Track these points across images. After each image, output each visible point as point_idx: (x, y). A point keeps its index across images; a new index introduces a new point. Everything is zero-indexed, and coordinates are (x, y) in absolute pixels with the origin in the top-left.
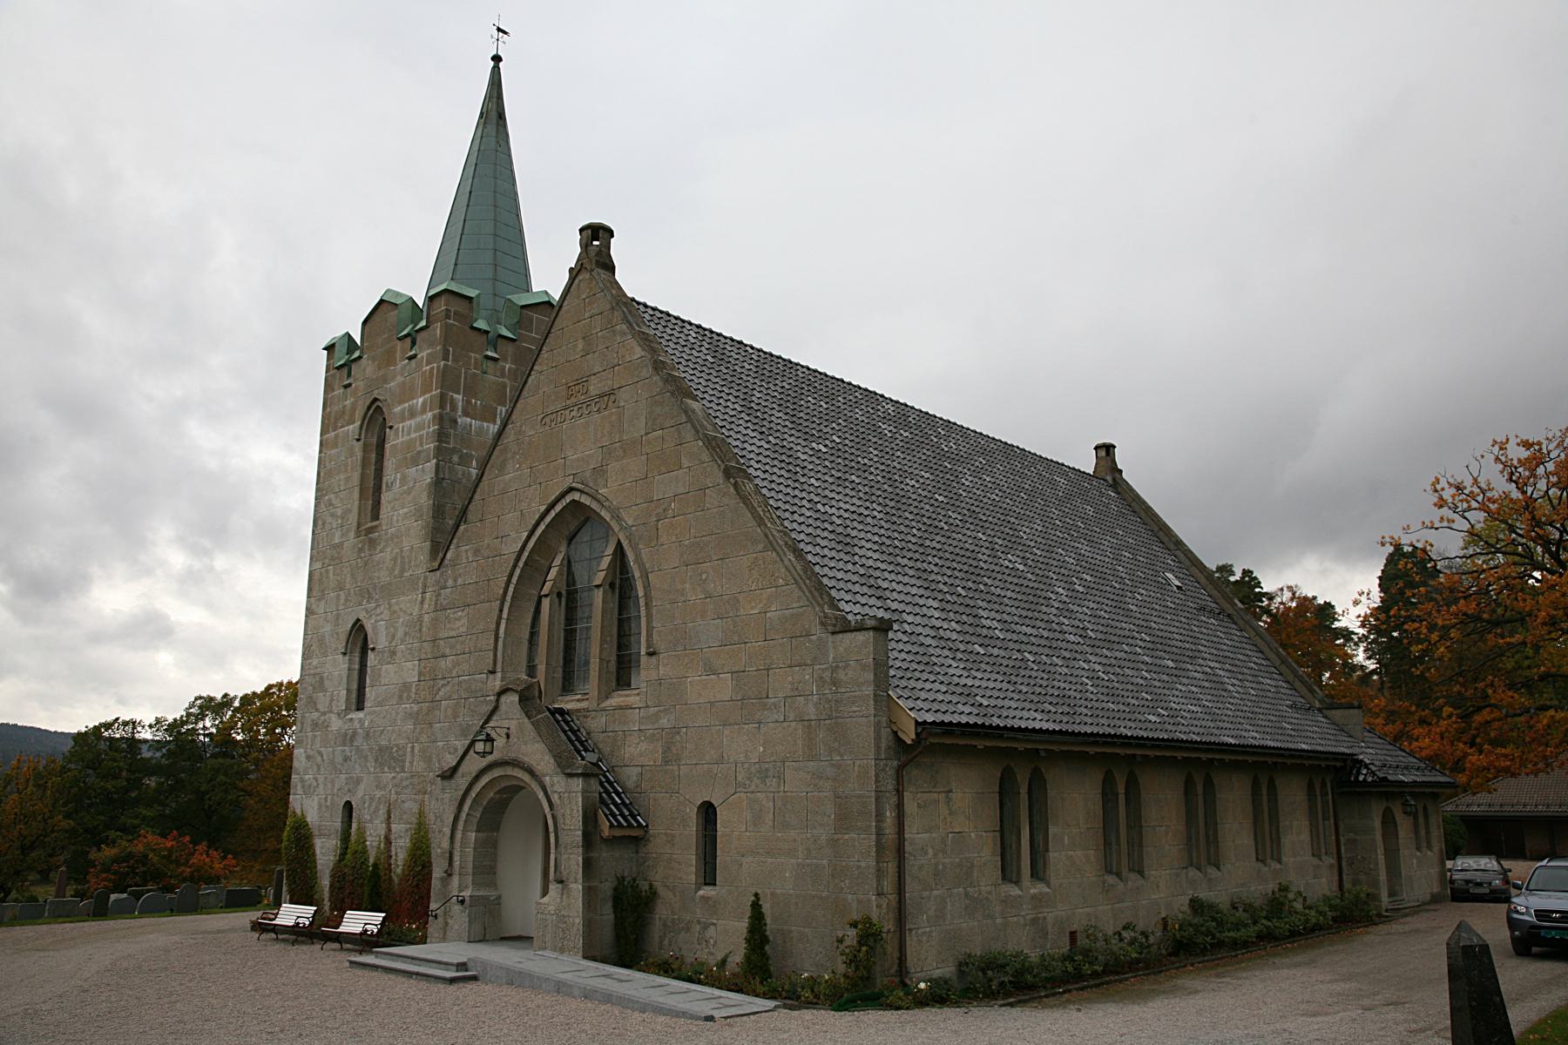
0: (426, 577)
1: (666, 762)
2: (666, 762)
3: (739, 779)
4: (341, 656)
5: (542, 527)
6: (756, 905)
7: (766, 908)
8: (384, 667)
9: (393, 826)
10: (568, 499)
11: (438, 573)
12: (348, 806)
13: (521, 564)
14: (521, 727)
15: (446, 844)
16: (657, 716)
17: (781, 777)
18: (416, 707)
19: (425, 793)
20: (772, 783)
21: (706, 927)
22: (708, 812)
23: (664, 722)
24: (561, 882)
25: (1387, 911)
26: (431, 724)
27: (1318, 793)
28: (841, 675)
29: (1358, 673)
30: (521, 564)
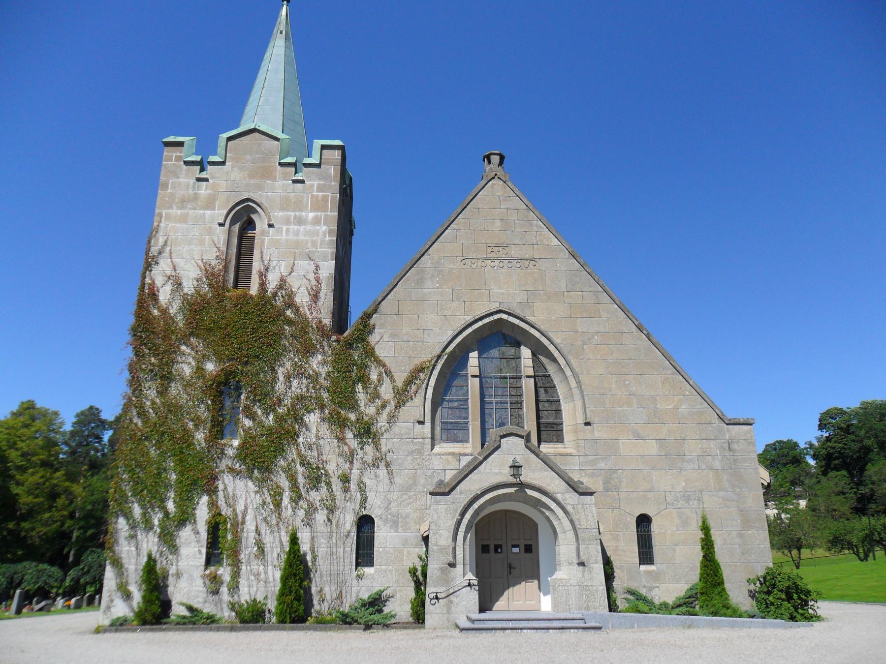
3: (669, 500)
10: (496, 317)
17: (700, 500)
23: (602, 465)
24: (581, 564)
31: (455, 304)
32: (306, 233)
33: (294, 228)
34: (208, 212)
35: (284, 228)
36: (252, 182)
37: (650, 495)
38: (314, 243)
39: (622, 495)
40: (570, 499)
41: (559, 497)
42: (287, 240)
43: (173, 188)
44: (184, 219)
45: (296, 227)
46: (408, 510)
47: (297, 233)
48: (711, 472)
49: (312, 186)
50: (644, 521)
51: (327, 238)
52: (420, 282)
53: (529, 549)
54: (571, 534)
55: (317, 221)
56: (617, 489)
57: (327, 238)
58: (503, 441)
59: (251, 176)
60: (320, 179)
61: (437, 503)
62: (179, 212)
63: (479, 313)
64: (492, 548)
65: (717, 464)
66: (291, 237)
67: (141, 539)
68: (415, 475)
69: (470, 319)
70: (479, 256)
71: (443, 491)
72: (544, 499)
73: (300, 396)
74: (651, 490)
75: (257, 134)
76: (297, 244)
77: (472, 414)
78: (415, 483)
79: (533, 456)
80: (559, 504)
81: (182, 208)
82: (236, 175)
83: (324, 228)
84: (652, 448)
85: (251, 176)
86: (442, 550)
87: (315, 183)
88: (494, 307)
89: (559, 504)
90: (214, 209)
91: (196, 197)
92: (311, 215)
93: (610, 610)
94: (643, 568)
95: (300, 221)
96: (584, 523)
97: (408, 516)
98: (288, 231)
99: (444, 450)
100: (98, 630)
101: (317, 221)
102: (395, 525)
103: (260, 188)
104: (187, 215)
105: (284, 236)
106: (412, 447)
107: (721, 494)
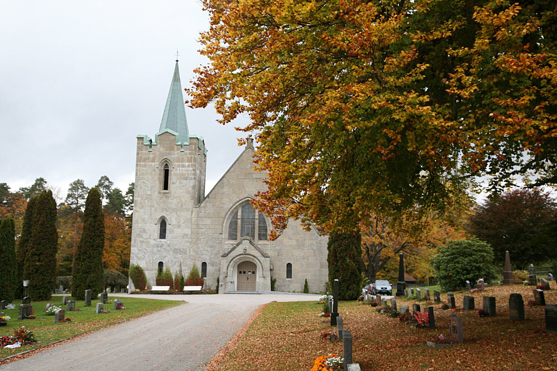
0: (192, 209)
1: (278, 255)
2: (278, 255)
3: (298, 259)
4: (154, 225)
5: (238, 204)
6: (306, 281)
7: (307, 281)
8: (175, 229)
9: (182, 268)
10: (247, 199)
11: (198, 209)
12: (161, 264)
13: (231, 211)
14: (250, 247)
15: (225, 270)
16: (275, 247)
17: (308, 259)
18: (190, 240)
19: (196, 260)
20: (306, 260)
21: (289, 285)
22: (289, 266)
23: (277, 248)
24: (264, 277)
25: (407, 291)
26: (197, 244)
27: (257, 222)
28: (322, 242)
29: (399, 137)
30: (231, 211)
31: (234, 194)
32: (186, 171)
33: (181, 168)
34: (153, 163)
35: (178, 168)
36: (167, 152)
37: (292, 257)
38: (188, 174)
39: (283, 257)
40: (262, 259)
41: (259, 258)
42: (179, 173)
43: (141, 154)
44: (145, 166)
45: (182, 168)
46: (217, 261)
47: (182, 171)
48: (312, 251)
49: (187, 153)
50: (289, 266)
51: (192, 172)
52: (222, 187)
53: (253, 273)
54: (261, 269)
55: (189, 166)
56: (281, 255)
57: (192, 172)
58: (243, 241)
59: (166, 150)
60: (190, 150)
61: (223, 259)
62: (143, 163)
63: (241, 198)
64: (242, 273)
65: (315, 248)
66: (181, 172)
67: (479, 287)
68: (219, 250)
69: (238, 200)
70: (242, 178)
71: (225, 256)
72: (254, 259)
73: (135, 270)
74: (293, 256)
75: (168, 134)
76: (183, 174)
77: (56, 296)
78: (219, 253)
79: (252, 246)
80: (259, 260)
81: (144, 162)
82: (162, 149)
83: (191, 168)
84: (294, 243)
85: (166, 150)
86: (224, 273)
87: (188, 152)
88: (246, 196)
89: (259, 260)
90: (155, 162)
91: (149, 158)
92: (187, 164)
93: (272, 290)
94: (288, 279)
95: (183, 166)
96: (266, 266)
97: (216, 263)
98: (179, 170)
99: (228, 243)
100: (176, 78)
101: (189, 166)
102: (213, 265)
103: (170, 154)
104: (146, 164)
105: (178, 172)
106: (218, 242)
107: (315, 257)
